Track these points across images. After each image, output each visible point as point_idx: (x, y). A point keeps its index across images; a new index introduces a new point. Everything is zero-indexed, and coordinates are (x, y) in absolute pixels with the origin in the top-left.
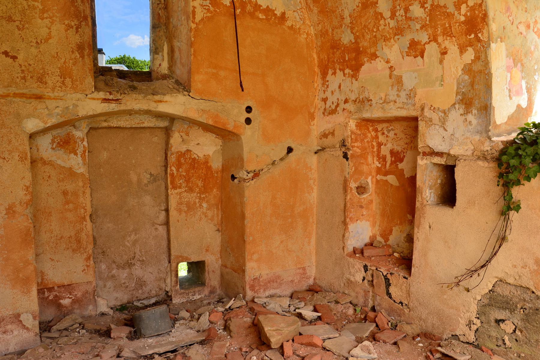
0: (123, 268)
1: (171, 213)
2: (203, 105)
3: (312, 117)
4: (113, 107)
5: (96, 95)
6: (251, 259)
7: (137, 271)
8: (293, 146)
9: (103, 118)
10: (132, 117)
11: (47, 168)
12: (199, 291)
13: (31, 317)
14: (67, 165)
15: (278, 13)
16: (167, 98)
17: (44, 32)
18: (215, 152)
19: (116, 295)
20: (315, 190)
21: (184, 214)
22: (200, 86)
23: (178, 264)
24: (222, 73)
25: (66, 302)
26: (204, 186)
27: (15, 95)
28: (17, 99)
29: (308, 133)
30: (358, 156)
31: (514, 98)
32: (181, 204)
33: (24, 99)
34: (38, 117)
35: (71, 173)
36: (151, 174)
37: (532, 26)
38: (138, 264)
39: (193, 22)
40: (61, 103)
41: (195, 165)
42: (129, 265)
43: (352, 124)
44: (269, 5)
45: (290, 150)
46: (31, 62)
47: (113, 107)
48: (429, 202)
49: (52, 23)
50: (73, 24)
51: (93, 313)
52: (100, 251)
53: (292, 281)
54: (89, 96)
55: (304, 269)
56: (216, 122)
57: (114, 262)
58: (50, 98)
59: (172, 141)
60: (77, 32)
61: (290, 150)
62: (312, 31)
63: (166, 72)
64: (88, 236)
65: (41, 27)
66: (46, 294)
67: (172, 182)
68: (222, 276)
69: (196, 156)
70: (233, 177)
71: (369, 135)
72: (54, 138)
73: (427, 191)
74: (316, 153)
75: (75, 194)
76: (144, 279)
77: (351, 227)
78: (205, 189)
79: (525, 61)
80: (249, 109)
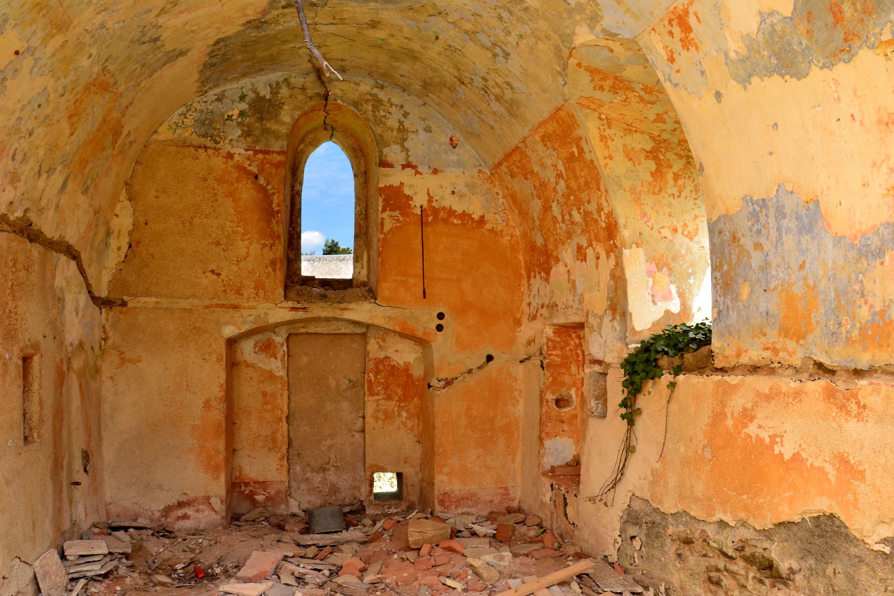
0: (318, 472)
1: (366, 420)
2: (390, 312)
3: (518, 323)
4: (300, 315)
5: (285, 304)
6: (441, 472)
7: (332, 476)
8: (494, 354)
9: (301, 325)
10: (329, 324)
11: (250, 371)
12: (395, 504)
13: (219, 501)
14: (268, 368)
15: (476, 217)
16: (353, 306)
17: (243, 251)
18: (416, 359)
19: (309, 498)
20: (522, 402)
21: (381, 422)
22: (387, 293)
23: (373, 473)
24: (412, 281)
25: (260, 498)
26: (404, 395)
27: (217, 306)
28: (218, 309)
29: (512, 341)
30: (557, 365)
31: (659, 304)
32: (379, 411)
33: (223, 309)
34: (234, 324)
35: (270, 376)
36: (350, 381)
37: (680, 230)
38: (333, 469)
39: (381, 233)
40: (254, 312)
41: (395, 374)
42: (323, 469)
43: (549, 331)
44: (465, 209)
45: (490, 358)
46: (232, 278)
47: (300, 315)
48: (596, 414)
49: (250, 243)
50: (268, 243)
51: (285, 513)
52: (296, 453)
53: (491, 501)
54: (279, 305)
55: (506, 489)
56: (403, 329)
57: (309, 465)
58: (244, 308)
59: (369, 348)
60: (271, 249)
61: (490, 358)
62: (518, 233)
63: (365, 279)
64: (283, 436)
65: (241, 247)
66: (243, 488)
67: (370, 389)
68: (421, 491)
69: (395, 363)
70: (429, 386)
71: (572, 343)
72: (257, 342)
73: (592, 401)
74: (521, 362)
75: (274, 396)
76: (338, 486)
77: (548, 443)
78: (405, 398)
79: (673, 265)
80: (441, 316)
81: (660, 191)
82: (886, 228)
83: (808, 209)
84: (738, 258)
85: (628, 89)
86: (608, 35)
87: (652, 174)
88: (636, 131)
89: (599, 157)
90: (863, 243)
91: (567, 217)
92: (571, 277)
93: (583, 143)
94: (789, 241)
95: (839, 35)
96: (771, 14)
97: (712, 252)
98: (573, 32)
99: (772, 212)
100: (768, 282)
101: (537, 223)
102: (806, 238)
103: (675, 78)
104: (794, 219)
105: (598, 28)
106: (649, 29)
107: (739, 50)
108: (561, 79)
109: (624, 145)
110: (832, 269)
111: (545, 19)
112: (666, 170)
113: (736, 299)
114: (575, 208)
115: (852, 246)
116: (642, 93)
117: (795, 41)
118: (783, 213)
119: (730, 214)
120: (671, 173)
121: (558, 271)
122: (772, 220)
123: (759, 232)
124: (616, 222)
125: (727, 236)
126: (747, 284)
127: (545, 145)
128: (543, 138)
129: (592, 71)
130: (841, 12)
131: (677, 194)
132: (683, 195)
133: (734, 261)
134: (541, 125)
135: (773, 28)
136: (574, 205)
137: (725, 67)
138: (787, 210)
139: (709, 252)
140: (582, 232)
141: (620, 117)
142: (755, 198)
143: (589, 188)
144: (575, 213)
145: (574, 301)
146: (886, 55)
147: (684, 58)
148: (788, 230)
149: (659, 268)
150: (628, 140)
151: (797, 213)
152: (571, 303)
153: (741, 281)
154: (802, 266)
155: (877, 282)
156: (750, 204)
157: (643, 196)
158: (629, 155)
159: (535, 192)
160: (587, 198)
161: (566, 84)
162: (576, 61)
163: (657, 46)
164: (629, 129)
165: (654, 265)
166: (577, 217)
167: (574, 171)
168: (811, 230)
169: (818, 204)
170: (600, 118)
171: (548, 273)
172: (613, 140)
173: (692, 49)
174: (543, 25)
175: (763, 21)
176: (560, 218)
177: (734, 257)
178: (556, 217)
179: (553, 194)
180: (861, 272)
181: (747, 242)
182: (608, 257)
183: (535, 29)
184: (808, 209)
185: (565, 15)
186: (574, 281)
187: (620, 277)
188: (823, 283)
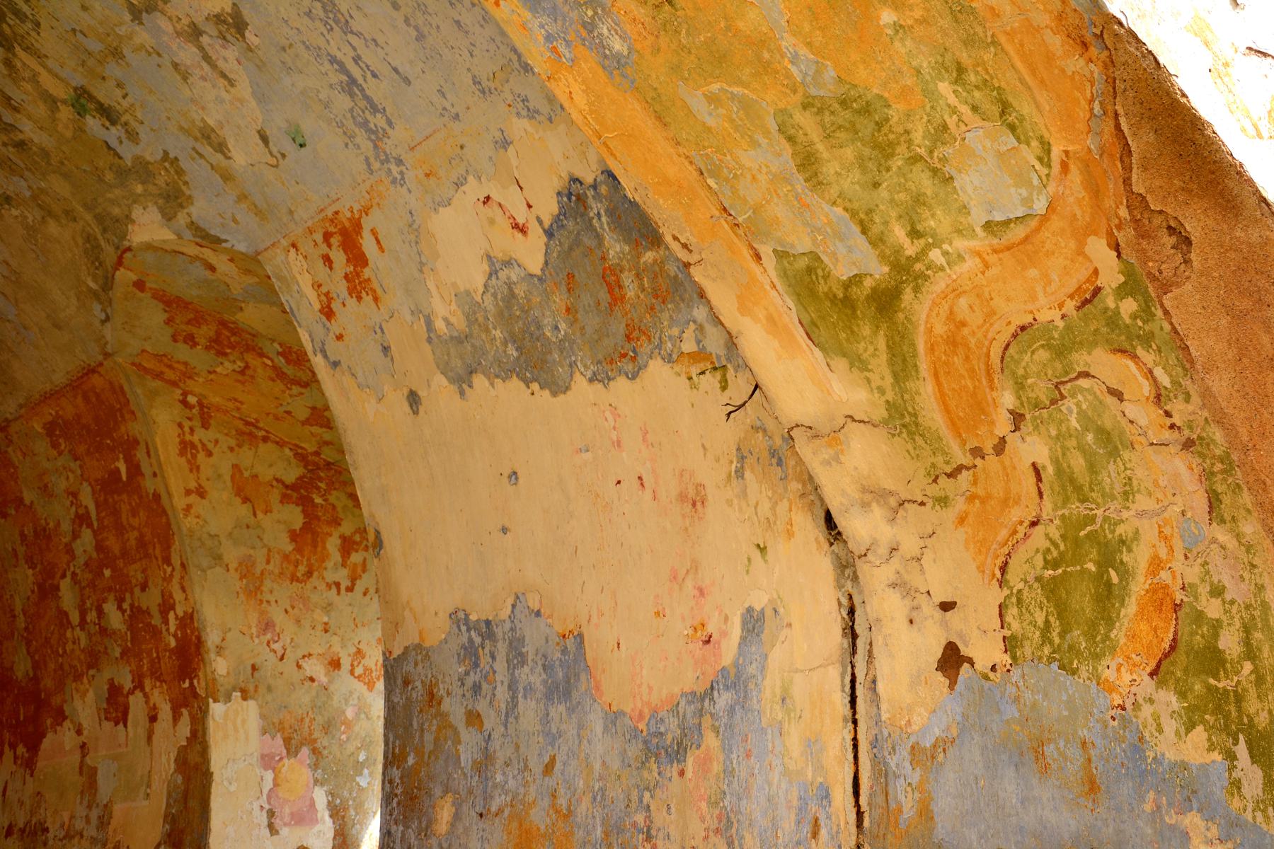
31: (284, 831)
37: (346, 663)
79: (323, 741)
81: (309, 574)
82: (689, 703)
83: (564, 651)
84: (436, 740)
85: (249, 348)
86: (202, 238)
87: (294, 536)
88: (265, 439)
89: (173, 489)
90: (653, 730)
91: (92, 616)
92: (88, 760)
93: (140, 454)
94: (529, 711)
95: (619, 328)
96: (508, 263)
97: (389, 724)
98: (128, 217)
99: (502, 648)
100: (487, 798)
101: (21, 622)
102: (558, 710)
103: (333, 347)
104: (539, 668)
105: (182, 219)
106: (284, 243)
107: (453, 320)
108: (97, 308)
109: (235, 466)
110: (601, 778)
111: (66, 176)
112: (326, 529)
113: (426, 831)
114: (111, 597)
115: (636, 733)
116: (281, 361)
117: (547, 321)
118: (521, 654)
119: (427, 644)
120: (336, 535)
121: (60, 743)
122: (500, 665)
123: (476, 688)
124: (199, 638)
125: (418, 691)
126: (449, 798)
127: (55, 445)
128: (50, 428)
129: (171, 303)
130: (620, 287)
131: (345, 583)
132: (359, 587)
133: (429, 746)
134: (47, 397)
135: (510, 289)
136: (110, 589)
137: (427, 348)
138: (529, 649)
139: (381, 722)
140: (123, 654)
141: (231, 405)
142: (473, 617)
143: (147, 556)
144: (110, 607)
145: (88, 821)
146: (690, 379)
147: (350, 313)
148: (529, 689)
149: (291, 748)
150: (246, 457)
151: (545, 656)
152: (79, 824)
153: (438, 791)
154: (549, 768)
155: (673, 810)
156: (464, 628)
157: (268, 584)
158: (245, 489)
159: (21, 550)
160: (140, 576)
161: (107, 319)
162: (133, 277)
163: (302, 279)
164: (249, 433)
165: (279, 740)
166: (116, 620)
167: (116, 513)
168: (567, 694)
169: (582, 642)
170: (184, 402)
171: (34, 747)
172: (210, 454)
173: (368, 299)
174: (60, 187)
175: (493, 273)
176: (75, 618)
177: (429, 738)
178: (66, 614)
179: (66, 558)
180: (647, 789)
181: (454, 708)
182: (176, 717)
183: (42, 190)
184: (564, 651)
185: (109, 176)
186: (94, 771)
187: (197, 767)
188: (583, 806)
